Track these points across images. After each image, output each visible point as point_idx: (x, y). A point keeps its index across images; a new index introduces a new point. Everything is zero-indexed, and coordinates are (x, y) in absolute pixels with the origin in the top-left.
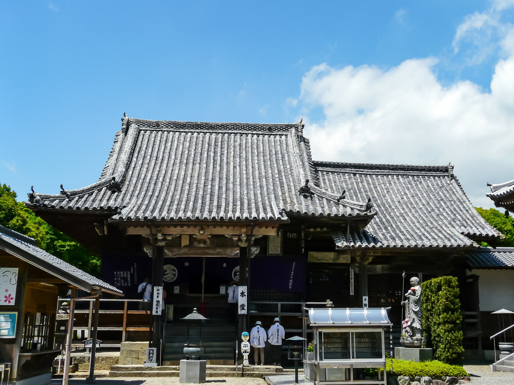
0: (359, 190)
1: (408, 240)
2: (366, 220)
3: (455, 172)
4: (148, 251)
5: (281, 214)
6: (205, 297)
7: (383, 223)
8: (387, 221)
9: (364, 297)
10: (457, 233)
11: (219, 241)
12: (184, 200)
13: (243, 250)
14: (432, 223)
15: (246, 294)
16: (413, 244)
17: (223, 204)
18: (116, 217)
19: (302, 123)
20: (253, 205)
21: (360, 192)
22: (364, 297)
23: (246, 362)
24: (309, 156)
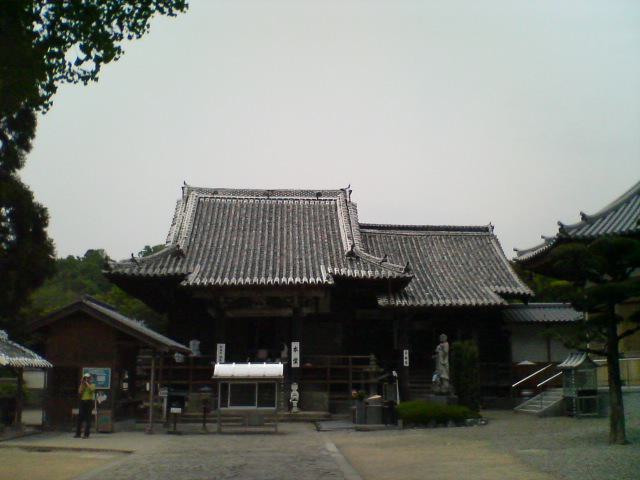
0: (403, 251)
1: (444, 299)
2: (405, 281)
3: (495, 232)
4: (212, 312)
5: (328, 278)
6: (150, 365)
7: (423, 283)
8: (427, 281)
10: (491, 293)
11: (275, 302)
12: (243, 265)
13: (296, 311)
14: (468, 282)
16: (448, 302)
17: (278, 269)
18: (184, 283)
20: (305, 269)
21: (404, 253)
23: (295, 409)
24: (357, 221)
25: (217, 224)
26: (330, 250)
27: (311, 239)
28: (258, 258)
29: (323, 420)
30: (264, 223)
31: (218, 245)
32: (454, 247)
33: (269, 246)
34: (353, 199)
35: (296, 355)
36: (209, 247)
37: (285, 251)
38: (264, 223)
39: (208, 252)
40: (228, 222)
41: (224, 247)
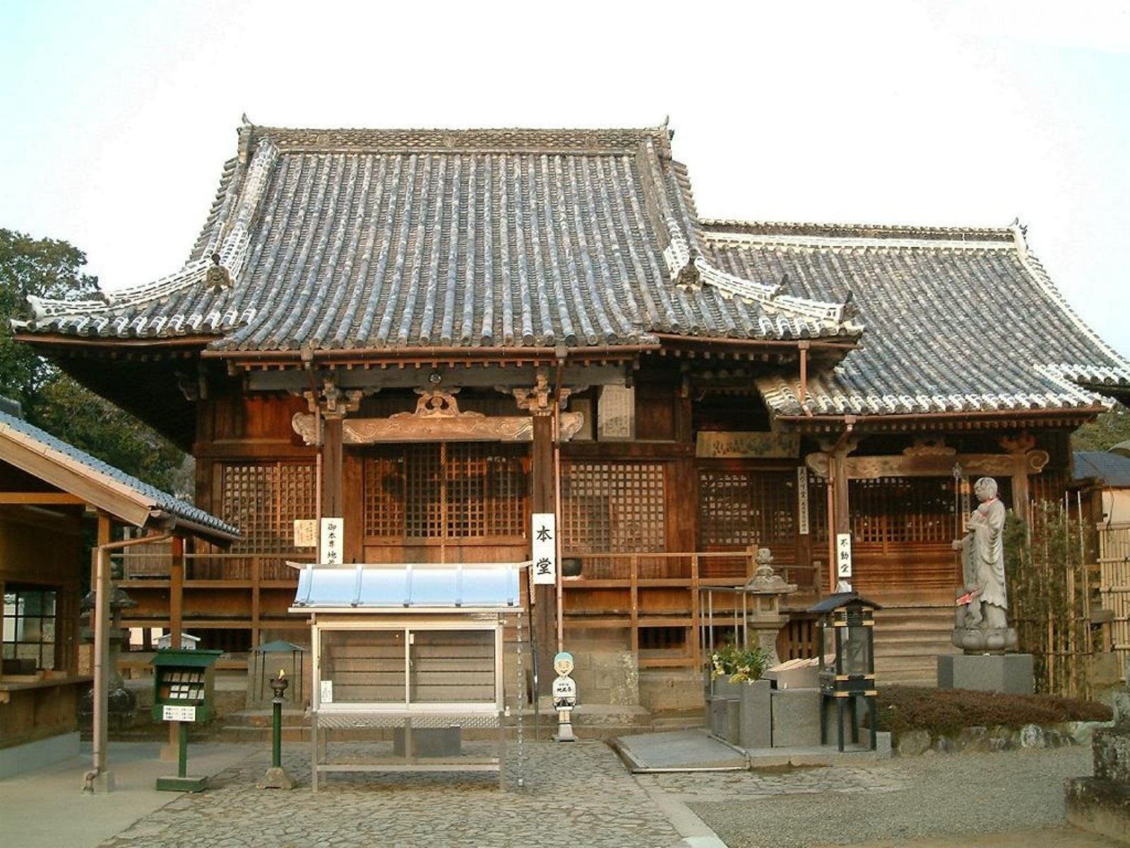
9: (840, 537)
15: (551, 533)
19: (669, 127)
20: (563, 310)
22: (840, 537)
25: (323, 213)
26: (631, 269)
27: (574, 243)
28: (431, 287)
29: (634, 732)
30: (446, 206)
31: (324, 259)
32: (936, 276)
33: (461, 258)
34: (678, 152)
35: (544, 550)
36: (300, 264)
37: (505, 271)
38: (446, 206)
39: (295, 275)
40: (353, 207)
41: (340, 262)
